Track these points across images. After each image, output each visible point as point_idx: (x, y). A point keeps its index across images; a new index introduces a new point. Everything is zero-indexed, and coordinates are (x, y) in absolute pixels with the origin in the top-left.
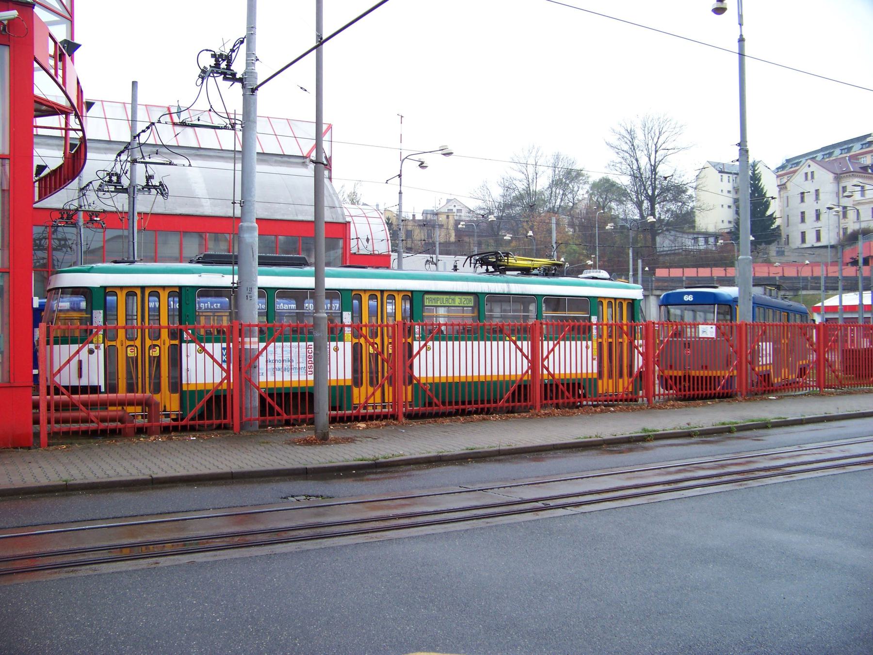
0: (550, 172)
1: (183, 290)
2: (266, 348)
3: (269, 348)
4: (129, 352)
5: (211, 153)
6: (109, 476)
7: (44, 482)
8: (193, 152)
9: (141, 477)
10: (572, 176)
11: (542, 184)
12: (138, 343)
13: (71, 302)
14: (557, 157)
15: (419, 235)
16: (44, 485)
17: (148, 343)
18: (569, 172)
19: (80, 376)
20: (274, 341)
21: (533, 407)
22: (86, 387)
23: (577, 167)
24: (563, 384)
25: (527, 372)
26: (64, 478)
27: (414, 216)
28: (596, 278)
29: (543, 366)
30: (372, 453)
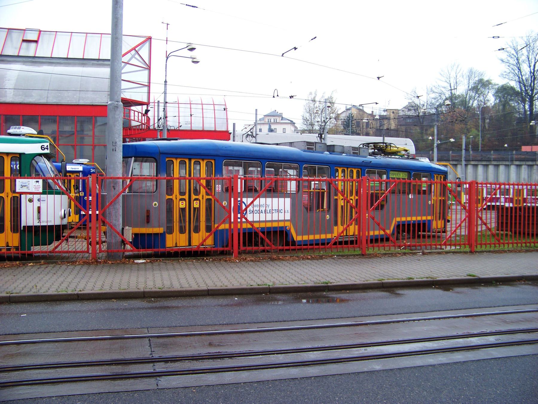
0: (466, 82)
1: (22, 156)
2: (252, 202)
3: (255, 203)
4: (180, 204)
5: (44, 60)
6: (274, 283)
7: (177, 287)
8: (30, 59)
9: (230, 287)
10: (481, 85)
11: (461, 90)
12: (186, 197)
13: (83, 168)
14: (471, 72)
15: (376, 125)
16: (176, 290)
17: (194, 197)
18: (481, 81)
19: (39, 218)
20: (259, 197)
21: (230, 253)
22: (46, 226)
23: (485, 79)
24: (263, 233)
25: (465, 219)
26: (226, 284)
27: (372, 112)
28: (19, 135)
29: (478, 216)
30: (272, 280)
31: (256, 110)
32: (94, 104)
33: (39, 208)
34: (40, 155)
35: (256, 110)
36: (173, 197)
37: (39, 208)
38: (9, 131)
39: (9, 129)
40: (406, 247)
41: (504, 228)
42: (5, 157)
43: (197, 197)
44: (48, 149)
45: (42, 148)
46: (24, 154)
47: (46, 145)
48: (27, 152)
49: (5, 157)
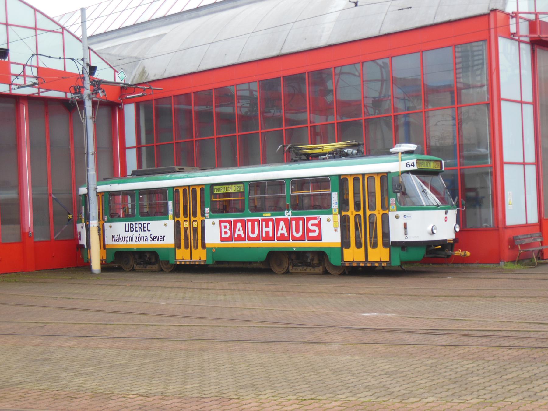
17: (193, 219)
31: (411, 8)
32: (287, 50)
33: (405, 225)
34: (407, 172)
35: (411, 8)
36: (375, 212)
37: (405, 225)
38: (392, 150)
39: (393, 147)
40: (470, 359)
41: (480, 53)
42: (376, 177)
43: (186, 219)
44: (414, 165)
45: (407, 165)
46: (390, 172)
47: (411, 162)
48: (392, 171)
49: (376, 177)
